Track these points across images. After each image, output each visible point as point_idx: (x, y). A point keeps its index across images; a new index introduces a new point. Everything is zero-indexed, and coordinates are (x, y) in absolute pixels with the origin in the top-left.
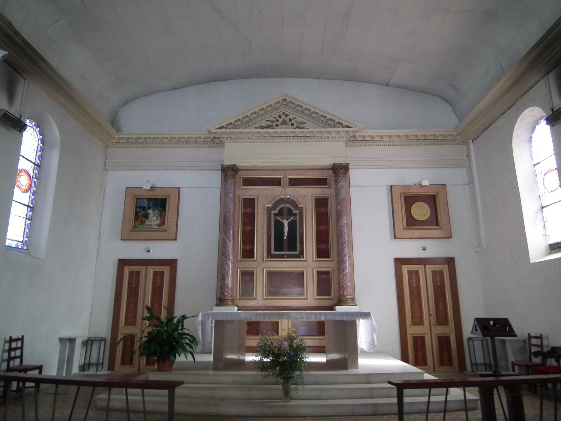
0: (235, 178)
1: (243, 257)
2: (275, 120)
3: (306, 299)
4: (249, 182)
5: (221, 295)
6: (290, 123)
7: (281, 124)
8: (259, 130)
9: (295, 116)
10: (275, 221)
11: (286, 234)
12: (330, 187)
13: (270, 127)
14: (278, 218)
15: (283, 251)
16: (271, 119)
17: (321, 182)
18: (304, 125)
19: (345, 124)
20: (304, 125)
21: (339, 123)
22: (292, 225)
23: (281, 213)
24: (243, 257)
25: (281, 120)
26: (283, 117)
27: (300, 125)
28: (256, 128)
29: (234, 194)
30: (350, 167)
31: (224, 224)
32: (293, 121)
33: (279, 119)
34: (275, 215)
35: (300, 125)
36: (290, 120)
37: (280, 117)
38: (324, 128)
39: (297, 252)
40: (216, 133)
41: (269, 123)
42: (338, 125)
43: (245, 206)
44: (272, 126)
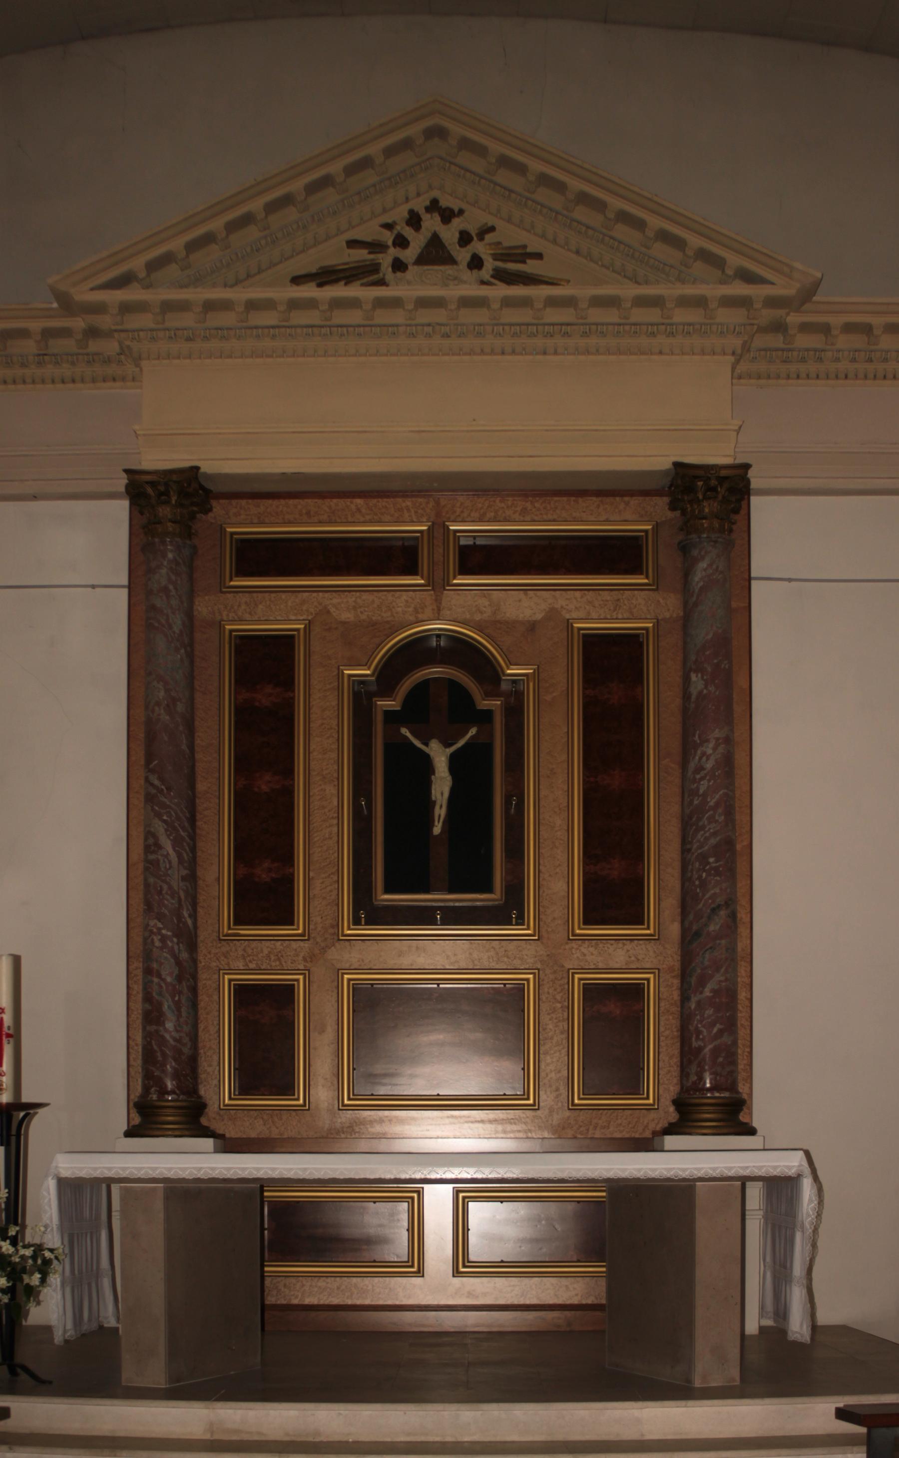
0: (190, 536)
1: (240, 919)
2: (388, 237)
3: (572, 937)
4: (266, 557)
5: (146, 1089)
6: (463, 255)
7: (422, 260)
8: (309, 291)
9: (491, 221)
10: (388, 748)
11: (440, 812)
12: (656, 586)
13: (366, 273)
14: (405, 731)
15: (427, 891)
16: (370, 231)
17: (612, 555)
18: (530, 267)
19: (734, 260)
20: (530, 267)
21: (704, 255)
22: (470, 769)
23: (417, 709)
24: (240, 919)
25: (417, 241)
26: (431, 223)
27: (512, 266)
28: (297, 280)
29: (190, 615)
30: (755, 484)
31: (148, 761)
32: (479, 247)
33: (408, 232)
34: (389, 716)
35: (512, 266)
36: (465, 239)
37: (414, 221)
38: (635, 280)
39: (493, 898)
40: (99, 309)
41: (362, 255)
42: (699, 267)
43: (245, 676)
44: (375, 268)
